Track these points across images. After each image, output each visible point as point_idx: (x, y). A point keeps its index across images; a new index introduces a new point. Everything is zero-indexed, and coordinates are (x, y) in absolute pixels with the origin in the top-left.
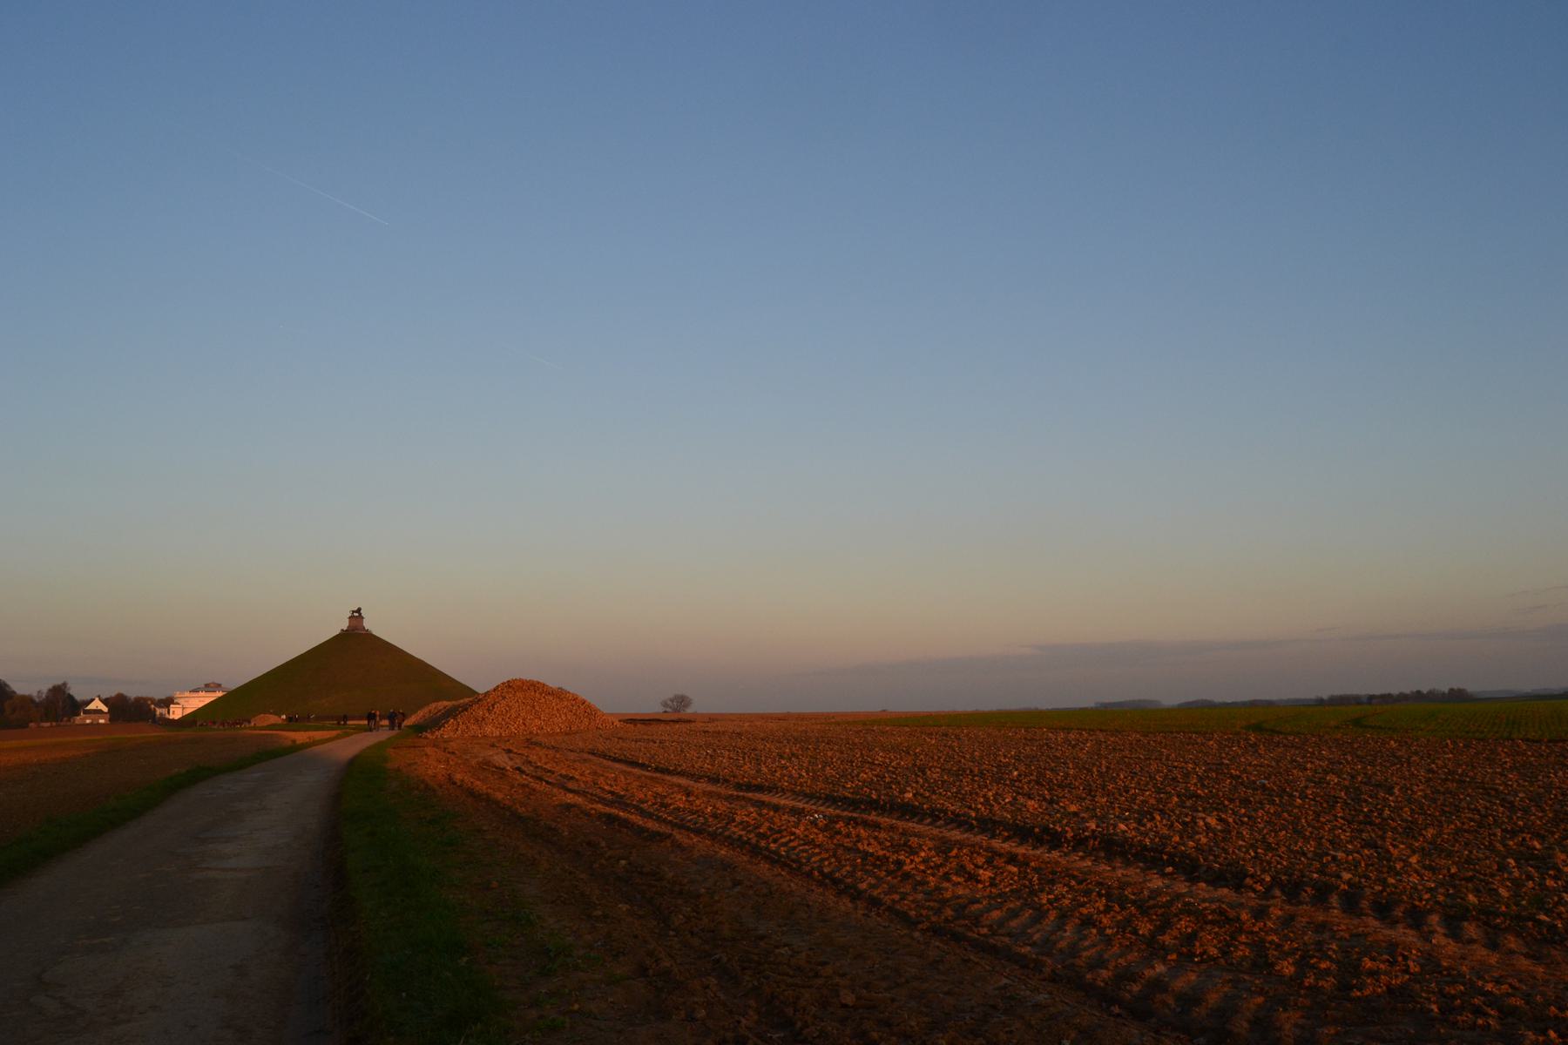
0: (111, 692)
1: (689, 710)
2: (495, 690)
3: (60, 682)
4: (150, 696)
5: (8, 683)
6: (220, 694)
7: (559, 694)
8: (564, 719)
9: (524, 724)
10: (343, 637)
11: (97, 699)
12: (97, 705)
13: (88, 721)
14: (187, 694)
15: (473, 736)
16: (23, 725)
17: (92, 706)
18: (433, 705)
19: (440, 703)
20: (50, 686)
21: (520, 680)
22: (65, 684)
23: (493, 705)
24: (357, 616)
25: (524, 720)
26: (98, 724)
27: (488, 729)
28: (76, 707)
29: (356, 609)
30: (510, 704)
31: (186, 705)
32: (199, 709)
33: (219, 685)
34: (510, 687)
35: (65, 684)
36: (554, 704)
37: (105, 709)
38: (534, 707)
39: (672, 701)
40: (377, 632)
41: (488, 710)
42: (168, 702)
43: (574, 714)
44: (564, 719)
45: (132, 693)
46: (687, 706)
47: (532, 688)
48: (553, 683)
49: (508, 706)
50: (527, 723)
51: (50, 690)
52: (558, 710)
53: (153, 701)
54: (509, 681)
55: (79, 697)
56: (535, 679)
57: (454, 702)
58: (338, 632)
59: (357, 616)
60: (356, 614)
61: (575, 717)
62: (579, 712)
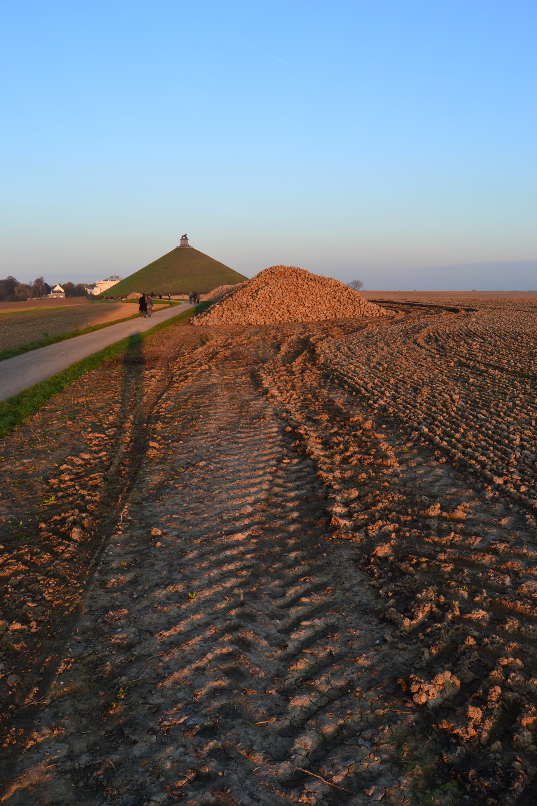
0: (65, 282)
1: (361, 289)
2: (258, 276)
3: (39, 277)
4: (85, 283)
5: (15, 278)
6: (118, 282)
7: (321, 281)
8: (328, 305)
9: (289, 311)
10: (178, 250)
11: (58, 285)
12: (58, 288)
13: (55, 297)
14: (102, 282)
15: (237, 324)
16: (24, 299)
17: (56, 289)
18: (220, 287)
19: (224, 286)
20: (35, 279)
21: (282, 267)
22: (42, 278)
23: (257, 291)
24: (184, 238)
25: (288, 307)
26: (60, 298)
27: (253, 317)
28: (48, 289)
29: (184, 235)
30: (274, 291)
31: (102, 287)
32: (108, 289)
33: (118, 277)
34: (272, 273)
35: (42, 278)
36: (317, 290)
37: (62, 290)
38: (297, 293)
39: (352, 284)
40: (195, 247)
41: (252, 296)
42: (93, 286)
43: (338, 301)
44: (328, 305)
45: (76, 282)
46: (359, 287)
47: (294, 274)
48: (315, 270)
49: (271, 292)
50: (292, 309)
51: (35, 281)
52: (321, 296)
53: (86, 285)
54: (271, 268)
55: (50, 284)
56: (296, 265)
57: (233, 286)
58: (175, 248)
59: (184, 238)
60: (184, 238)
61: (339, 303)
62: (342, 298)
